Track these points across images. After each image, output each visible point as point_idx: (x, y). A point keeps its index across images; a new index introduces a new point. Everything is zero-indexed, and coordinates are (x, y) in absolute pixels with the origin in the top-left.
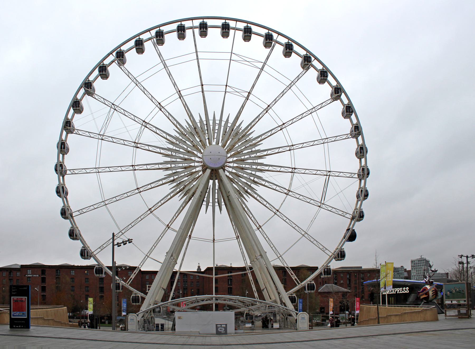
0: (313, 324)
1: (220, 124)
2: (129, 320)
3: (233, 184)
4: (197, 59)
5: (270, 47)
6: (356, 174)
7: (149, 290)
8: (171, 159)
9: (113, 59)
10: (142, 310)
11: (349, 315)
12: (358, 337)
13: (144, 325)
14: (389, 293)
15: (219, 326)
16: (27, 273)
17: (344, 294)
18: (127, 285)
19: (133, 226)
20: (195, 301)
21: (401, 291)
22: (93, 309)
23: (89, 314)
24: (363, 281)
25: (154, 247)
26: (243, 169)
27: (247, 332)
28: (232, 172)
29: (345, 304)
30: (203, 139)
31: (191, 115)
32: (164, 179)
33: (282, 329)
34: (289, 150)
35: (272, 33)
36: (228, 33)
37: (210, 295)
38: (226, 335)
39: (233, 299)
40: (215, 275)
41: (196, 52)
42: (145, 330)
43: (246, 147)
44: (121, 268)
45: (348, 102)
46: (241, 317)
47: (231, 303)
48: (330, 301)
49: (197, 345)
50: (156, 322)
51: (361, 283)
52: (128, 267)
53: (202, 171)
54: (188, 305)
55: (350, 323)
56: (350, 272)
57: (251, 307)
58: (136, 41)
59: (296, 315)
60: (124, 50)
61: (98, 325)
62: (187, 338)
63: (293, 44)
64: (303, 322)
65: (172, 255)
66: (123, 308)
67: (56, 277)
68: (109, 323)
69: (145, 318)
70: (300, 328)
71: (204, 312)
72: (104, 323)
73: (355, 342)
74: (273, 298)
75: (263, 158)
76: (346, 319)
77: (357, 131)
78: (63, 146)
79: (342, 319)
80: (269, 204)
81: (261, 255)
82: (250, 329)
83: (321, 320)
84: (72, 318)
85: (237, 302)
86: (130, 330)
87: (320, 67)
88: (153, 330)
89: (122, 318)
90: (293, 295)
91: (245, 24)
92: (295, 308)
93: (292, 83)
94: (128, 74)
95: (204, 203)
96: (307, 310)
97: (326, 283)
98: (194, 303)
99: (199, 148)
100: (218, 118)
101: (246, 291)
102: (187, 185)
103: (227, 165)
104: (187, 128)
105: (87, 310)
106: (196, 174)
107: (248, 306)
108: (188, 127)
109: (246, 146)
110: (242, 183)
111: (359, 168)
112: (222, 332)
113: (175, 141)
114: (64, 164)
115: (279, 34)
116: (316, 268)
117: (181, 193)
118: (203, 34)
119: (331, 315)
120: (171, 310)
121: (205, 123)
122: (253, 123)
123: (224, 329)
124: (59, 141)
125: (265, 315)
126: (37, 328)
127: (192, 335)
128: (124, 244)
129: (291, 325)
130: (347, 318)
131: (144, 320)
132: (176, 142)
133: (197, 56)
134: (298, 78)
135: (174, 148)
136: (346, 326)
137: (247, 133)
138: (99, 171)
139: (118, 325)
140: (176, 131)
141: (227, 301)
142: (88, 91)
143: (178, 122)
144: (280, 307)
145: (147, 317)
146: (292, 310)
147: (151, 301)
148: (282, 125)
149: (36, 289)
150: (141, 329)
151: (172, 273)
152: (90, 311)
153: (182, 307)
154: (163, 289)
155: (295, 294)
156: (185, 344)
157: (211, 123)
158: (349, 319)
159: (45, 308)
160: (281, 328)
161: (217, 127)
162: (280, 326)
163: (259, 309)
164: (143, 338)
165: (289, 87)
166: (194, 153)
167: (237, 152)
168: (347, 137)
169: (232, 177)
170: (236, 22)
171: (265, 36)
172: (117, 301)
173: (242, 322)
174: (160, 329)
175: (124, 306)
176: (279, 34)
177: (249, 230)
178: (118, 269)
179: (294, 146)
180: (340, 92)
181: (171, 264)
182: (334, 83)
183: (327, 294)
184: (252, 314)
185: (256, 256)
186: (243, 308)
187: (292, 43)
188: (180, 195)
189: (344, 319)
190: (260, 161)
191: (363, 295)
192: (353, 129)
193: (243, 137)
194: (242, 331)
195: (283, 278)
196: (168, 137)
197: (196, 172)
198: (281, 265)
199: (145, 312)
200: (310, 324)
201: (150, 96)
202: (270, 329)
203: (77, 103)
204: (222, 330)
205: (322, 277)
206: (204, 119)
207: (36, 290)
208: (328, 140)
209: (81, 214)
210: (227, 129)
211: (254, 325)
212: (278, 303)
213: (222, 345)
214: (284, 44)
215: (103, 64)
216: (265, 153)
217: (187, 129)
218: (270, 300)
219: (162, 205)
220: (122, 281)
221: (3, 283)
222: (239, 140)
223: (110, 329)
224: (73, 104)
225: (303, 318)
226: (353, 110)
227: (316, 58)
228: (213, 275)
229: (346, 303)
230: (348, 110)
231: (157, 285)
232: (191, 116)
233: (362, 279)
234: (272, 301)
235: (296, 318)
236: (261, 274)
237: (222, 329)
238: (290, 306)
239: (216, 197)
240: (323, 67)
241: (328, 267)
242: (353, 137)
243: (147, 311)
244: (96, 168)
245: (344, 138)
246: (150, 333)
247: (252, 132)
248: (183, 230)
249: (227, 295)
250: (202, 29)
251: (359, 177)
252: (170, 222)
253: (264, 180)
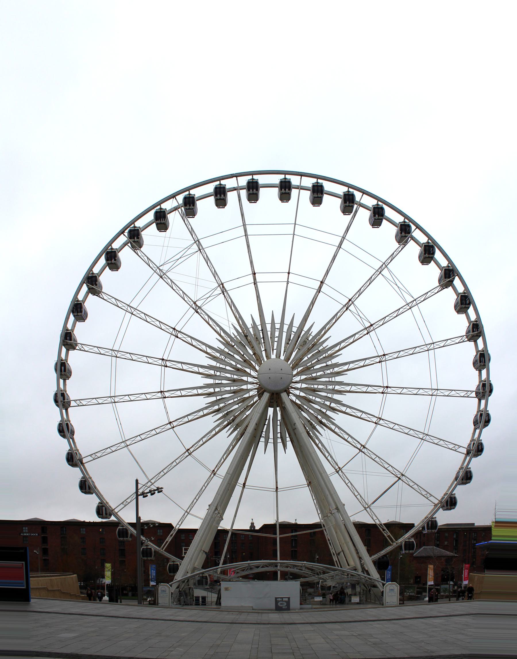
0: (405, 598)
1: (281, 329)
2: (159, 591)
3: (302, 412)
4: (246, 235)
5: (351, 213)
6: (473, 391)
7: (185, 553)
8: (215, 380)
10: (177, 580)
11: (454, 586)
12: (466, 615)
13: (179, 598)
15: (279, 599)
16: (23, 531)
17: (449, 559)
18: (161, 550)
19: (166, 473)
20: (247, 568)
22: (111, 578)
23: (107, 583)
24: (475, 542)
25: (195, 500)
26: (314, 390)
27: (316, 607)
28: (299, 396)
29: (450, 572)
30: (257, 351)
31: (240, 317)
32: (206, 408)
33: (363, 604)
34: (379, 362)
35: (353, 192)
36: (289, 195)
37: (268, 560)
38: (289, 611)
39: (298, 566)
40: (280, 534)
41: (244, 225)
42: (181, 605)
43: (319, 360)
44: (148, 526)
45: (463, 289)
46: (308, 588)
47: (295, 570)
48: (428, 568)
49: (251, 623)
50: (195, 595)
51: (473, 545)
52: (157, 524)
53: (258, 395)
54: (238, 573)
55: (454, 596)
57: (321, 576)
58: (156, 213)
59: (382, 587)
60: (139, 227)
61: (119, 597)
62: (237, 615)
63: (385, 206)
65: (216, 509)
66: (151, 576)
67: (61, 536)
68: (133, 595)
69: (181, 590)
70: (387, 603)
71: (259, 582)
72: (127, 595)
73: (461, 622)
74: (352, 563)
75: (343, 375)
76: (449, 592)
77: (475, 332)
78: (63, 368)
79: (444, 591)
80: (352, 437)
81: (337, 508)
82: (320, 603)
83: (416, 592)
84: (83, 589)
85: (304, 569)
86: (162, 605)
87: (423, 239)
88: (192, 605)
89: (150, 589)
91: (314, 180)
92: (381, 577)
93: (384, 265)
94: (148, 262)
95: (262, 439)
96: (397, 579)
97: (424, 546)
98: (246, 570)
99: (252, 364)
100: (278, 320)
101: (315, 555)
102: (238, 415)
103: (293, 386)
104: (236, 337)
105: (104, 578)
106: (251, 400)
107: (318, 574)
108: (236, 334)
109: (319, 359)
110: (314, 410)
111: (477, 383)
113: (218, 355)
114: (66, 392)
115: (364, 192)
116: (411, 525)
117: (230, 427)
118: (253, 197)
119: (429, 587)
120: (215, 579)
121: (260, 328)
122: (329, 325)
123: (285, 604)
124: (57, 361)
125: (340, 586)
126: (39, 601)
127: (243, 611)
128: (152, 494)
129: (375, 599)
130: (452, 591)
131: (180, 591)
132: (220, 357)
133: (245, 231)
134: (392, 257)
135: (218, 365)
136: (450, 601)
137: (319, 340)
138: (116, 401)
139: (146, 597)
140: (220, 341)
141: (290, 568)
142: (93, 288)
143: (221, 329)
144: (361, 576)
145: (183, 588)
146: (377, 579)
147: (188, 568)
148: (369, 327)
149: (35, 551)
150: (175, 603)
151: (217, 532)
152: (108, 580)
153: (230, 576)
154: (204, 553)
155: (413, 538)
156: (234, 622)
157: (269, 327)
158: (454, 591)
159: (48, 576)
160: (361, 602)
161: (277, 334)
162: (360, 600)
163: (333, 578)
164: (179, 615)
165: (379, 271)
166: (245, 371)
167: (306, 368)
168: (461, 340)
169: (299, 403)
170: (301, 177)
171: (343, 197)
172: (143, 568)
173: (310, 594)
174: (201, 603)
175: (153, 573)
176: (364, 193)
177: (321, 474)
178: (144, 526)
179: (386, 356)
180: (452, 275)
181: (214, 520)
182: (444, 263)
183: (425, 560)
184: (323, 584)
185: (330, 510)
186: (311, 577)
187: (382, 205)
188: (229, 429)
189: (447, 592)
190: (338, 379)
191: (474, 560)
192: (470, 328)
193: (315, 346)
194: (310, 606)
195: (366, 538)
196: (209, 351)
197: (249, 397)
198: (370, 521)
199: (181, 581)
200: (401, 597)
201: (181, 292)
202: (348, 604)
203: (79, 306)
204: (283, 605)
206: (258, 322)
207: (35, 552)
208: (435, 345)
209: (94, 459)
210: (291, 335)
211: (325, 599)
212: (359, 571)
213: (283, 624)
214: (371, 207)
215: (112, 249)
216: (346, 367)
217: (235, 338)
218: (348, 567)
219: (204, 443)
220: (149, 542)
222: (309, 350)
223: (136, 602)
224: (73, 308)
225: (392, 590)
226: (471, 300)
227: (418, 227)
228: (276, 534)
229: (451, 570)
230: (463, 301)
231: (197, 548)
232: (239, 318)
233: (474, 540)
234: (349, 568)
235: (382, 591)
236: (336, 533)
237: (284, 604)
238: (375, 574)
239: (279, 431)
240: (428, 240)
242: (469, 340)
243: (183, 580)
244: (112, 397)
245: (457, 342)
246: (188, 608)
247: (327, 339)
248: (232, 475)
249: (290, 560)
250: (251, 190)
251: (478, 396)
252: (217, 466)
253: (344, 405)
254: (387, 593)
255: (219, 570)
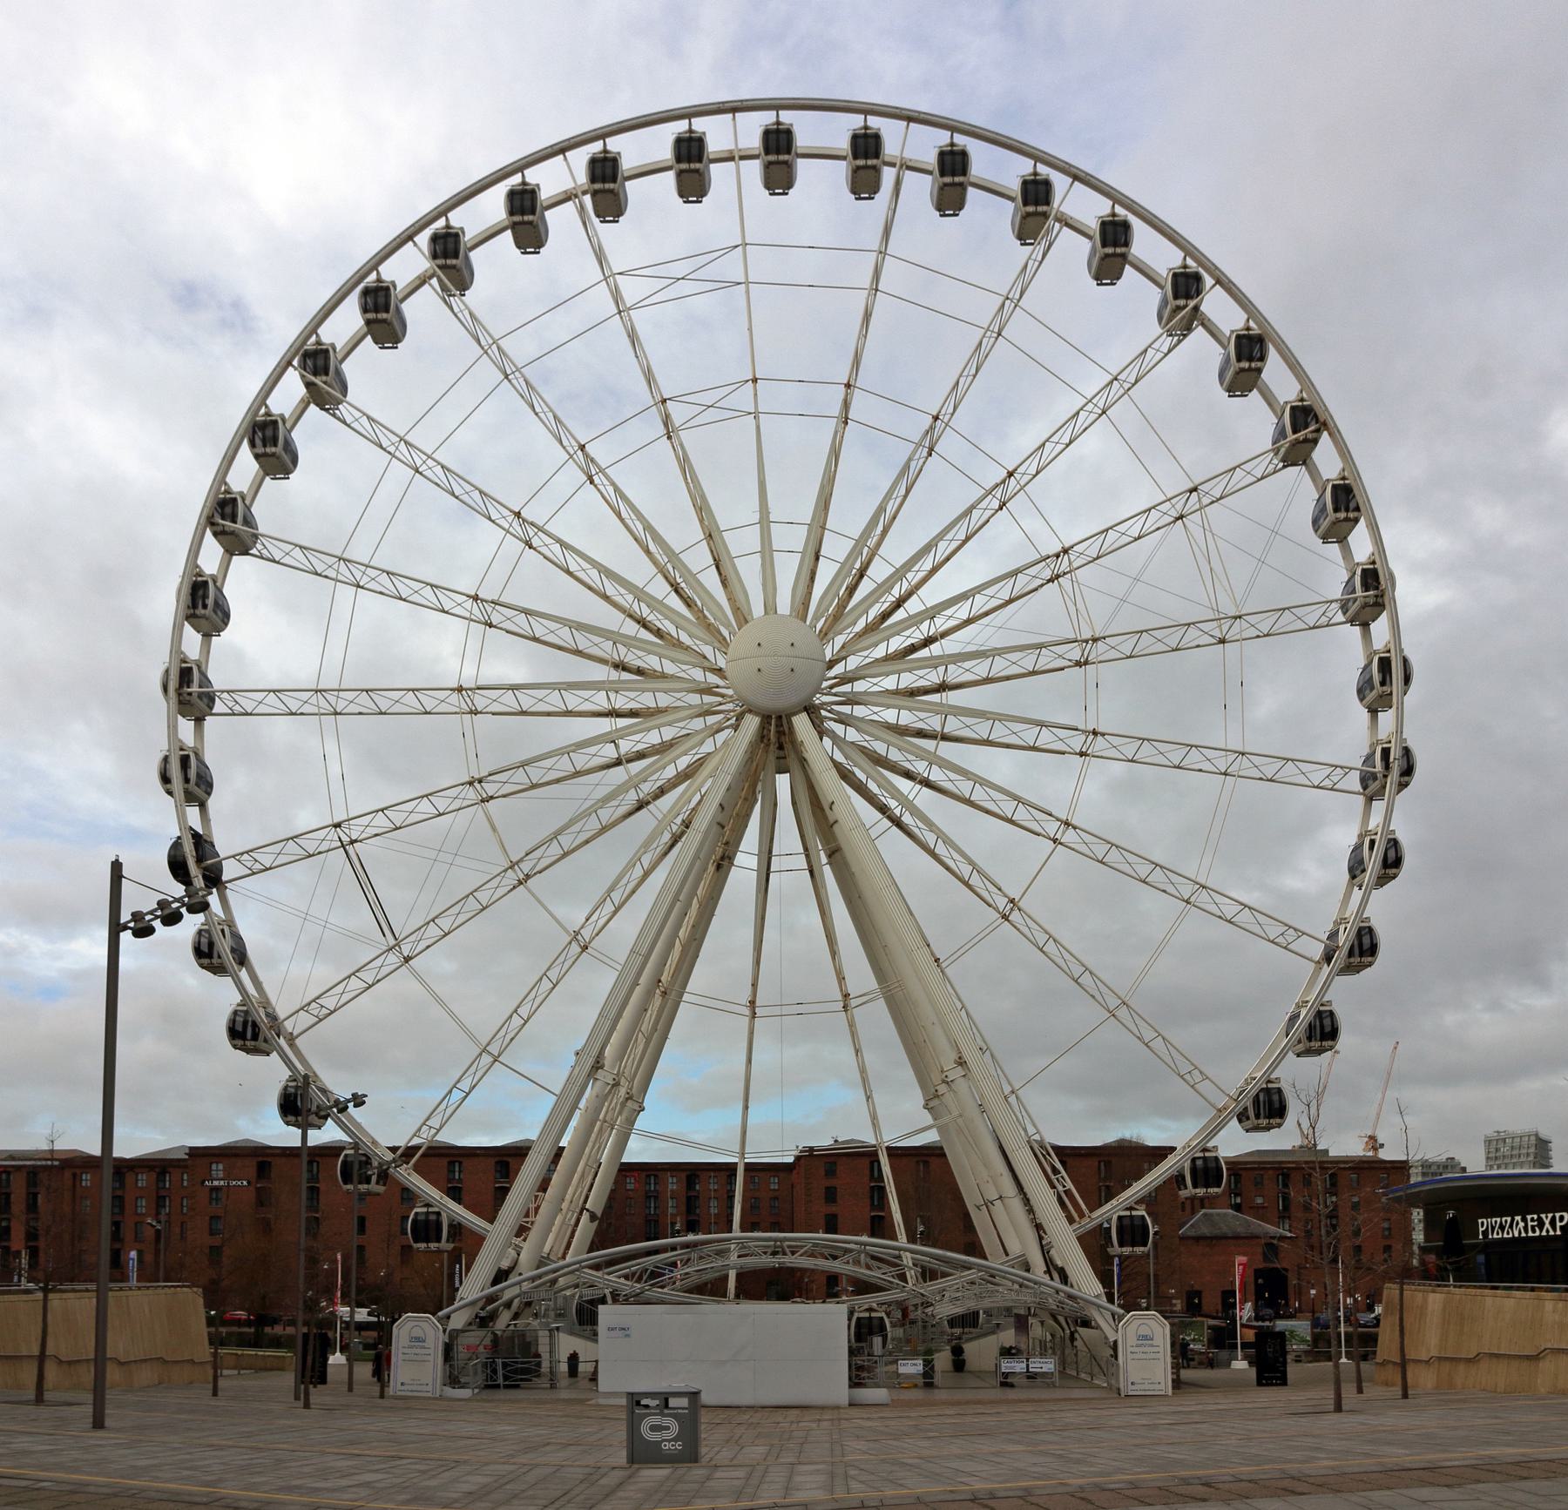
9: (424, 269)
14: (1523, 1235)
21: (1533, 1227)
56: (1288, 1168)
63: (1134, 220)
64: (1144, 1356)
74: (1015, 1247)
90: (1134, 1213)
97: (1203, 1208)
112: (666, 1446)
115: (1078, 176)
123: (674, 1427)
155: (1144, 1206)
165: (1101, 405)
168: (1324, 620)
176: (1076, 178)
204: (667, 1435)
205: (1183, 1193)
221: (139, 1211)
227: (1222, 281)
237: (668, 1428)
238: (1087, 1283)
241: (1207, 1154)
242: (1352, 621)
244: (320, 691)
254: (1130, 1349)
255: (734, 1257)
